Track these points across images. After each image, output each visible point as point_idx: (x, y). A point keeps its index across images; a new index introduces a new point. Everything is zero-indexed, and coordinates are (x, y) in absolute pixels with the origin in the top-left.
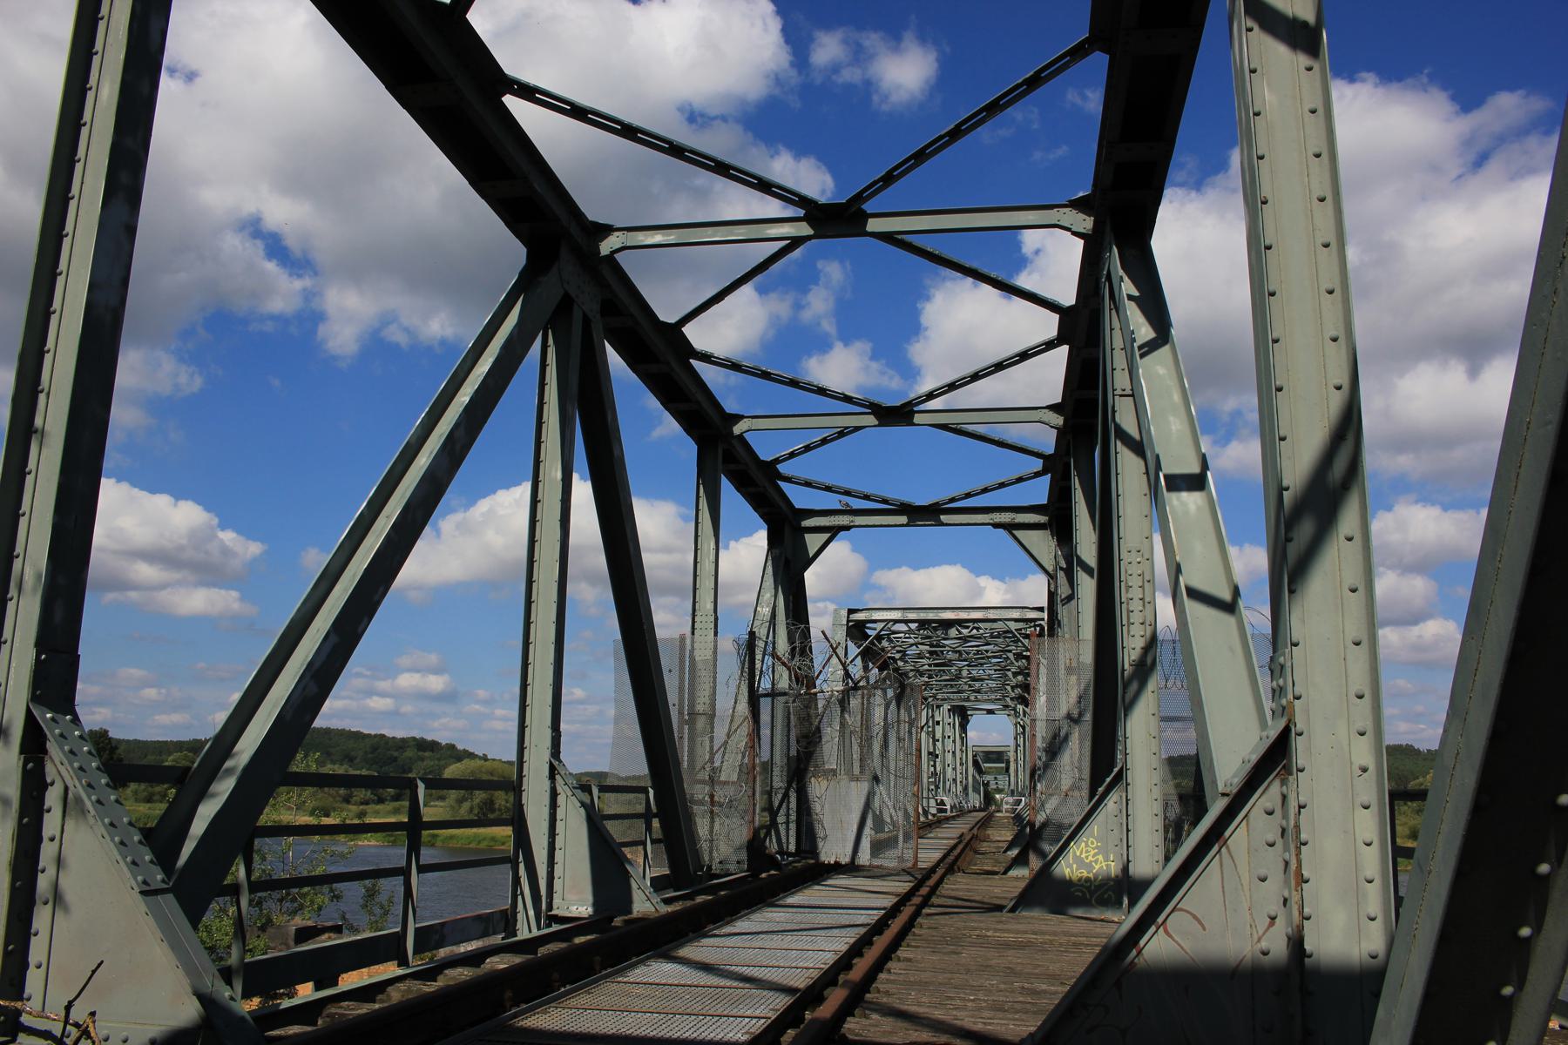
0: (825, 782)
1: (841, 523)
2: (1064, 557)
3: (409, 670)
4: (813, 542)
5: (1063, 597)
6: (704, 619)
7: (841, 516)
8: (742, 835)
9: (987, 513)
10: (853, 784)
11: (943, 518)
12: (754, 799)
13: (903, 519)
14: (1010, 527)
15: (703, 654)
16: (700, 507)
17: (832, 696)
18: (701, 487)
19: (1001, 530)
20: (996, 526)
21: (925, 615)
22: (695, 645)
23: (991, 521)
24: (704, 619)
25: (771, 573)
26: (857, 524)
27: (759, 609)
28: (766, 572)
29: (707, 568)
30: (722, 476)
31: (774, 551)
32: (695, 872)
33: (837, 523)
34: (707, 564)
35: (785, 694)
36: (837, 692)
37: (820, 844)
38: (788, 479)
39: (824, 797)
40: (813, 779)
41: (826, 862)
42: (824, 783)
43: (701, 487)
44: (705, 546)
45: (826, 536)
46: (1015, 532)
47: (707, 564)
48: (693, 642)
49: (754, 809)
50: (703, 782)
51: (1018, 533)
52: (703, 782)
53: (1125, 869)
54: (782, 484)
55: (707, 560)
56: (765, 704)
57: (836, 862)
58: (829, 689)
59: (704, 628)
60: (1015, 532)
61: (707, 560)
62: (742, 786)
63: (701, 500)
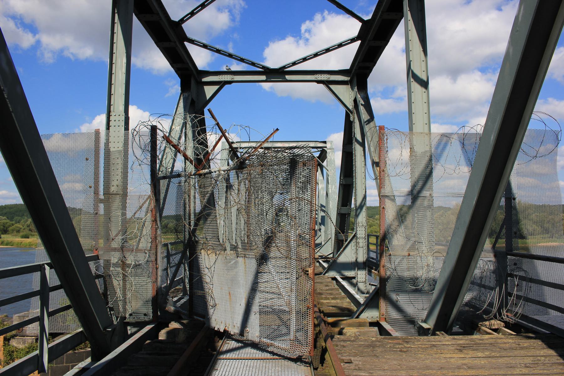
0: (214, 255)
1: (226, 80)
2: (362, 98)
3: (68, 182)
4: (209, 91)
5: (365, 120)
6: (117, 118)
7: (226, 76)
8: (150, 293)
9: (314, 75)
10: (240, 260)
11: (288, 77)
12: (156, 264)
13: (263, 78)
14: (327, 83)
15: (116, 145)
16: (115, 31)
17: (219, 175)
18: (116, 16)
19: (321, 85)
20: (319, 82)
21: (267, 145)
22: (110, 138)
23: (316, 79)
24: (117, 118)
25: (183, 106)
26: (235, 80)
27: (173, 127)
28: (179, 106)
29: (120, 78)
30: (134, 17)
31: (184, 94)
32: (105, 329)
33: (223, 80)
34: (120, 75)
35: (179, 176)
36: (224, 171)
37: (211, 311)
38: (192, 42)
39: (213, 269)
40: (203, 251)
41: (216, 329)
42: (213, 257)
43: (116, 16)
44: (119, 61)
45: (216, 87)
46: (331, 86)
47: (120, 75)
48: (108, 135)
49: (157, 272)
50: (115, 250)
51: (332, 87)
52: (115, 250)
53: (356, 260)
54: (186, 43)
55: (120, 72)
56: (163, 184)
57: (225, 331)
58: (217, 169)
59: (117, 126)
60: (331, 86)
61: (120, 72)
62: (146, 253)
63: (116, 25)
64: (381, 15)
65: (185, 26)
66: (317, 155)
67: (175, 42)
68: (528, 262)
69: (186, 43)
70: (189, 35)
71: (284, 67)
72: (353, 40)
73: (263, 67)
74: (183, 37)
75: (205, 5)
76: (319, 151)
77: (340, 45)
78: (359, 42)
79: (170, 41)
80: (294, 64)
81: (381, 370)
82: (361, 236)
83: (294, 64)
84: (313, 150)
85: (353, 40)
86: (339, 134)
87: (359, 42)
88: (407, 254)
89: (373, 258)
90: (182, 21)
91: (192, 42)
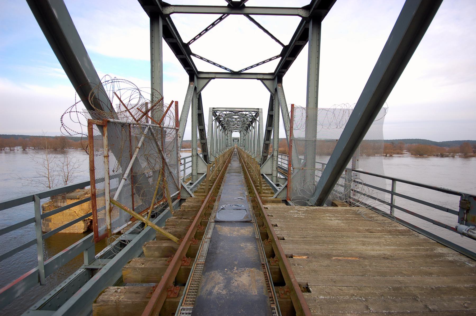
1: (212, 77)
14: (262, 80)
19: (259, 81)
20: (258, 79)
54: (191, 56)
64: (295, 43)
65: (191, 46)
66: (254, 115)
67: (186, 55)
68: (439, 220)
69: (191, 56)
70: (193, 51)
71: (241, 71)
72: (277, 57)
73: (231, 71)
74: (190, 53)
75: (215, 24)
76: (255, 113)
77: (270, 60)
78: (280, 58)
79: (183, 55)
80: (246, 69)
81: (339, 286)
82: (275, 155)
83: (246, 69)
84: (253, 112)
85: (277, 57)
86: (458, 204)
87: (280, 58)
88: (302, 168)
89: (279, 165)
90: (189, 43)
91: (194, 55)
